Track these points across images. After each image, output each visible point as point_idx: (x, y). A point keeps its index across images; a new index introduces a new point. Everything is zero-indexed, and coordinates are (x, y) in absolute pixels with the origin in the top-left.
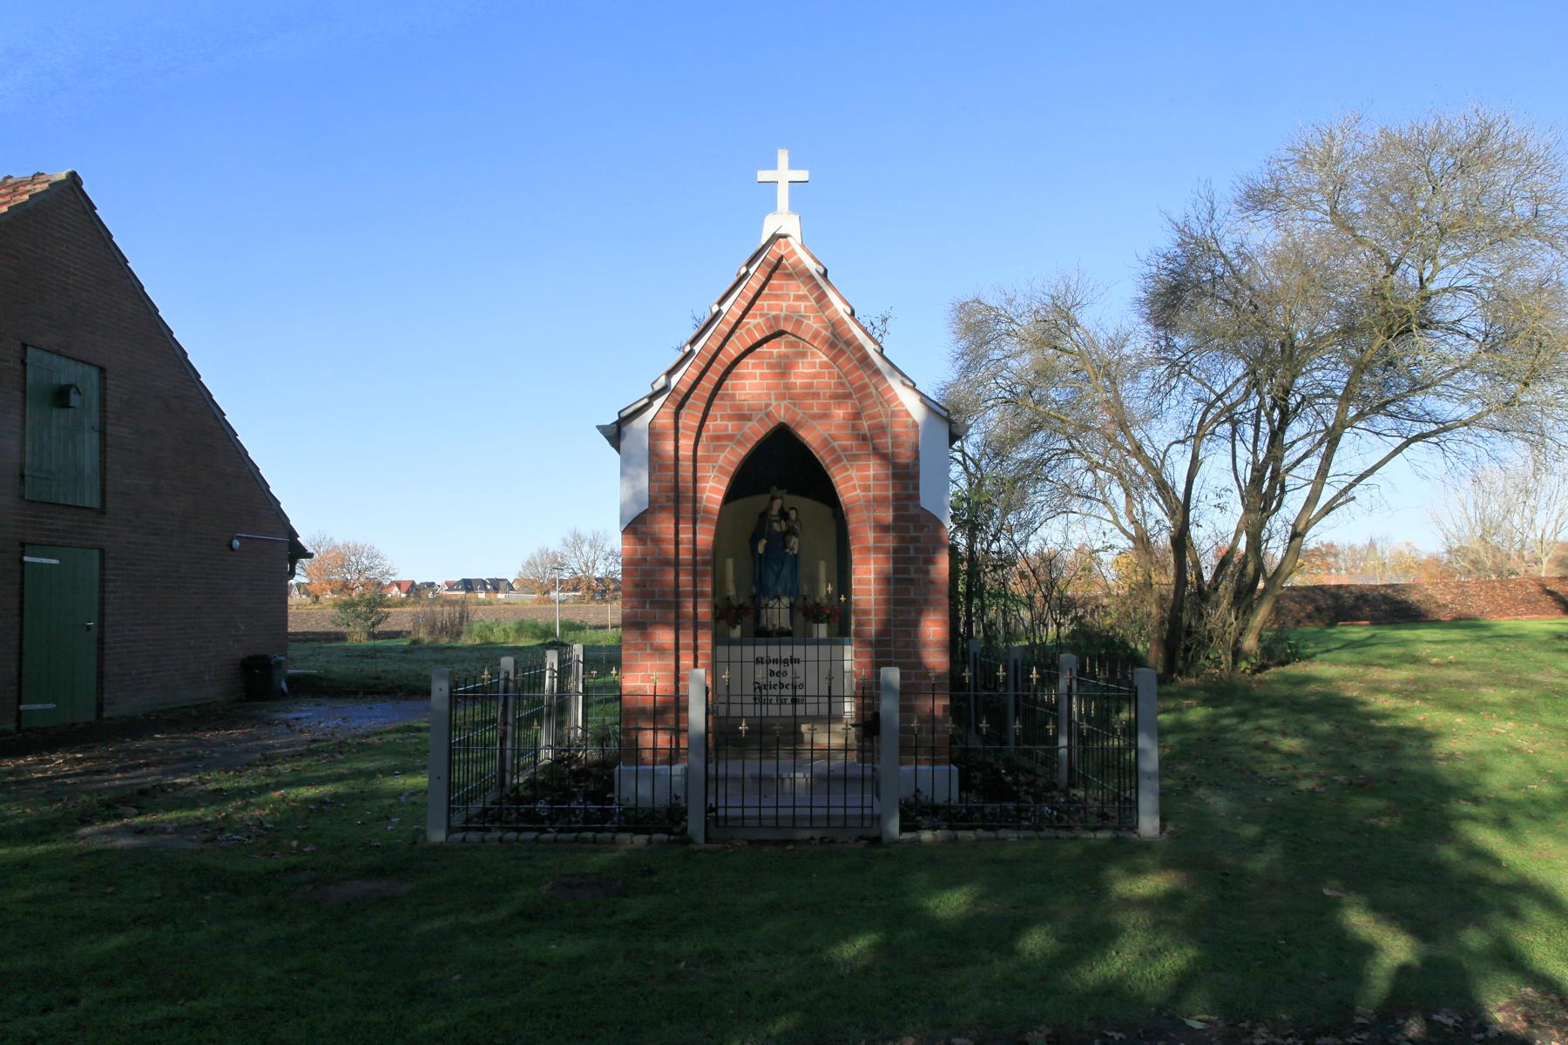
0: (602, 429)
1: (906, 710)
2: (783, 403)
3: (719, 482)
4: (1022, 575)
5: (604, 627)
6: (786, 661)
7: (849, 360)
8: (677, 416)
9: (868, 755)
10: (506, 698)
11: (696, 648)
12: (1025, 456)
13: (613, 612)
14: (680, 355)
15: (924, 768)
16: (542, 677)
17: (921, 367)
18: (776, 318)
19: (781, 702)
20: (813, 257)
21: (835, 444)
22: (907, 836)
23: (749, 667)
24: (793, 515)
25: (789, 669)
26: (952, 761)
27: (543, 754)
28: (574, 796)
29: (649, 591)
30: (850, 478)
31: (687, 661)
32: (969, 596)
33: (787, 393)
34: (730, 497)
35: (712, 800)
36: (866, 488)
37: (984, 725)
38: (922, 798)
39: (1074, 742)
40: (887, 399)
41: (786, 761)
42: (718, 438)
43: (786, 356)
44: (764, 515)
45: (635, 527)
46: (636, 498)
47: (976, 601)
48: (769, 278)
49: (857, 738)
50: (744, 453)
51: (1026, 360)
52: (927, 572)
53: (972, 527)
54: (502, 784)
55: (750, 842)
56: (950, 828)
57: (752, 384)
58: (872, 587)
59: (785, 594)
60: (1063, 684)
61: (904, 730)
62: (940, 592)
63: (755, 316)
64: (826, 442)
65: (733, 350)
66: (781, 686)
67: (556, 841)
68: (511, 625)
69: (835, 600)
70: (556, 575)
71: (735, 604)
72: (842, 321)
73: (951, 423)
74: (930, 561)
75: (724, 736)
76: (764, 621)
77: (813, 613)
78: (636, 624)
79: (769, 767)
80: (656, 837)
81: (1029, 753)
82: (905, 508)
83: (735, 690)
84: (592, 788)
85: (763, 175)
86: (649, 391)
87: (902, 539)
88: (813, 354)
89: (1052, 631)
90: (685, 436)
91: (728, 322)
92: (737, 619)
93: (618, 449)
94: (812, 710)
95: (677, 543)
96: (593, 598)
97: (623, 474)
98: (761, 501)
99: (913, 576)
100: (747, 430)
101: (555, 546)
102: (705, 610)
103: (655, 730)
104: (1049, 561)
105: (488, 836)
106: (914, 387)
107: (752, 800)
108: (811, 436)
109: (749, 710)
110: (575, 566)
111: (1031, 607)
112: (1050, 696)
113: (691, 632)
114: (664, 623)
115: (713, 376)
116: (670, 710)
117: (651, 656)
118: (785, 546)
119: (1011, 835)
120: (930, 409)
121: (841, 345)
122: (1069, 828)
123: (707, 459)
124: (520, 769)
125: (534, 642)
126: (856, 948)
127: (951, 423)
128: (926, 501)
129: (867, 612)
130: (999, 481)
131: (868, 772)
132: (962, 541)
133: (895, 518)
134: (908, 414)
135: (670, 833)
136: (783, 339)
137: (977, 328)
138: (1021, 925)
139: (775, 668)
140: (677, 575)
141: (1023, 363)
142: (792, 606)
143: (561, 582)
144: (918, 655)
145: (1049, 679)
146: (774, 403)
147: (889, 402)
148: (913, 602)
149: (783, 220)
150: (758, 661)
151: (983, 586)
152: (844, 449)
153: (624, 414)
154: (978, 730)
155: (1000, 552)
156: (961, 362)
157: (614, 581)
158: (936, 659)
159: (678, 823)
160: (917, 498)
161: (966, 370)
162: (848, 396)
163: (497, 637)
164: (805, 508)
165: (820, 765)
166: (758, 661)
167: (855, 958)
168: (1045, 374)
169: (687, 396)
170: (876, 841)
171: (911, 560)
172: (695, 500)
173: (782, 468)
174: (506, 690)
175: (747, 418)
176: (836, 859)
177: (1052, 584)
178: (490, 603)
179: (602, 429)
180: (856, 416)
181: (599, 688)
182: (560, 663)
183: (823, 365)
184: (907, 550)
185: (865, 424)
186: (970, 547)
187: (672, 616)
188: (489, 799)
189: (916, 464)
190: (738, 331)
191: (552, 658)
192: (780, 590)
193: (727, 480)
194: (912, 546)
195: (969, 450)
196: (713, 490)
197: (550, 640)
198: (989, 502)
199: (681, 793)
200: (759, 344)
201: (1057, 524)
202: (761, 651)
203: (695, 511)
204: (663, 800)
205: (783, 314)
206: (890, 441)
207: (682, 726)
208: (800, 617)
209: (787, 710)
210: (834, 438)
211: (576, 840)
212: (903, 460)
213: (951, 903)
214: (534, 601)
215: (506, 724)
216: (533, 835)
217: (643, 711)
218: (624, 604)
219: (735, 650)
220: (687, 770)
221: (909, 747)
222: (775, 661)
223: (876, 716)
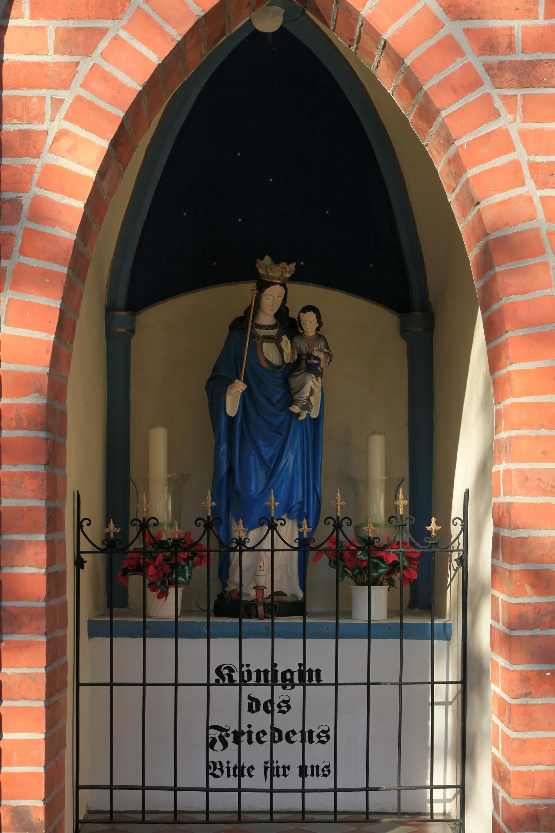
24: (309, 322)
30: (502, 143)
44: (241, 325)
66: (277, 735)
77: (359, 561)
118: (290, 397)
139: (262, 693)
142: (304, 546)
150: (224, 676)
166: (224, 676)
202: (225, 651)
208: (322, 570)
219: (161, 648)
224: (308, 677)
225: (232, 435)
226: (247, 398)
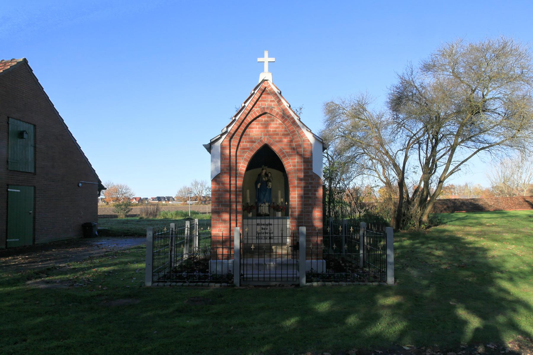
0: (205, 146)
1: (308, 241)
2: (266, 137)
3: (244, 164)
4: (348, 195)
5: (205, 213)
6: (267, 225)
7: (289, 122)
8: (230, 141)
9: (295, 256)
10: (172, 237)
11: (236, 220)
12: (348, 155)
13: (208, 208)
14: (231, 120)
15: (314, 261)
16: (184, 230)
17: (313, 125)
18: (264, 108)
19: (265, 238)
20: (276, 87)
21: (284, 151)
22: (308, 284)
23: (254, 227)
24: (270, 175)
25: (268, 227)
26: (324, 259)
27: (184, 256)
28: (195, 270)
29: (221, 201)
30: (289, 163)
31: (233, 225)
32: (329, 202)
33: (267, 134)
34: (248, 169)
35: (242, 272)
36: (294, 166)
37: (334, 246)
38: (313, 271)
39: (365, 252)
40: (301, 135)
41: (267, 259)
42: (244, 149)
43: (267, 121)
44: (260, 175)
45: (216, 179)
46: (216, 169)
47: (332, 204)
48: (261, 94)
49: (291, 251)
50: (253, 154)
51: (349, 122)
52: (315, 194)
53: (330, 179)
54: (171, 266)
55: (255, 286)
56: (323, 281)
57: (255, 130)
58: (297, 199)
59: (267, 202)
60: (361, 232)
61: (307, 248)
62: (320, 201)
63: (256, 107)
64: (281, 150)
65: (249, 119)
66: (266, 233)
67: (189, 286)
68: (174, 212)
69: (284, 204)
70: (189, 195)
71: (250, 205)
72: (286, 109)
73: (323, 144)
74: (316, 190)
75: (246, 250)
76: (260, 211)
77: (276, 208)
78: (216, 212)
79: (261, 260)
80: (223, 284)
81: (350, 256)
82: (308, 172)
83: (250, 234)
84: (201, 268)
85: (259, 60)
86: (221, 133)
87: (307, 183)
88: (276, 120)
89: (358, 214)
90: (233, 148)
91: (247, 110)
92: (251, 210)
93: (210, 153)
94: (276, 241)
95: (230, 184)
96: (202, 203)
97: (212, 161)
98: (259, 170)
99: (310, 196)
100: (254, 146)
101: (189, 185)
102: (239, 207)
103: (223, 248)
104: (356, 191)
105: (166, 284)
106: (311, 132)
107: (256, 272)
108: (276, 148)
109: (255, 241)
110: (196, 192)
111: (350, 206)
112: (357, 236)
113: (235, 215)
114: (226, 212)
115: (242, 128)
116: (228, 241)
117: (221, 223)
118: (267, 186)
119: (344, 284)
120: (316, 139)
121: (286, 117)
122: (363, 281)
123: (240, 156)
124: (177, 261)
125: (182, 218)
126: (291, 322)
127: (323, 144)
128: (315, 170)
129: (295, 208)
130: (340, 164)
131: (295, 262)
132: (327, 184)
133: (304, 176)
134: (309, 141)
135: (228, 283)
136: (266, 115)
137: (332, 111)
138: (347, 314)
139: (264, 227)
140: (230, 195)
141: (348, 123)
142: (269, 206)
143: (191, 198)
144: (312, 223)
145: (357, 231)
146: (263, 137)
147: (302, 137)
148: (310, 205)
149: (266, 75)
150: (258, 225)
151: (334, 199)
152: (287, 152)
153: (212, 141)
154: (333, 248)
155: (340, 188)
156: (327, 123)
157: (209, 197)
158: (318, 224)
159: (230, 280)
160: (312, 169)
161: (328, 126)
162: (288, 135)
163: (169, 216)
164: (274, 173)
165: (279, 260)
166: (258, 225)
167: (291, 325)
168: (355, 127)
169: (234, 135)
170: (298, 286)
171: (310, 190)
172: (236, 170)
173: (266, 159)
174: (172, 235)
175: (254, 142)
176: (284, 292)
177: (358, 198)
178: (167, 205)
179: (205, 146)
180: (291, 141)
181: (204, 234)
182: (190, 225)
183: (280, 124)
184: (308, 187)
185: (294, 144)
186: (330, 186)
187: (228, 209)
188: (166, 271)
189: (311, 158)
190: (251, 113)
191: (188, 224)
192: (265, 200)
193: (247, 163)
194: (310, 186)
195: (330, 153)
196: (242, 166)
197: (187, 217)
198: (336, 170)
199: (231, 269)
200: (258, 117)
201: (359, 178)
202: (259, 221)
203: (236, 174)
204: (225, 272)
205: (266, 107)
206: (302, 150)
207: (232, 246)
208: (272, 210)
209: (268, 241)
210: (284, 149)
211: (196, 285)
212: (307, 156)
213: (323, 307)
214: (182, 204)
215: (172, 246)
216: (181, 284)
217: (219, 242)
218: (212, 205)
219: (250, 221)
220: (233, 261)
221: (309, 254)
222: (263, 225)
223: (298, 243)
224: (270, 224)
225: (259, 191)
226: (260, 186)
